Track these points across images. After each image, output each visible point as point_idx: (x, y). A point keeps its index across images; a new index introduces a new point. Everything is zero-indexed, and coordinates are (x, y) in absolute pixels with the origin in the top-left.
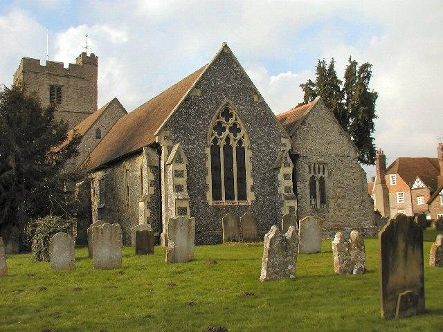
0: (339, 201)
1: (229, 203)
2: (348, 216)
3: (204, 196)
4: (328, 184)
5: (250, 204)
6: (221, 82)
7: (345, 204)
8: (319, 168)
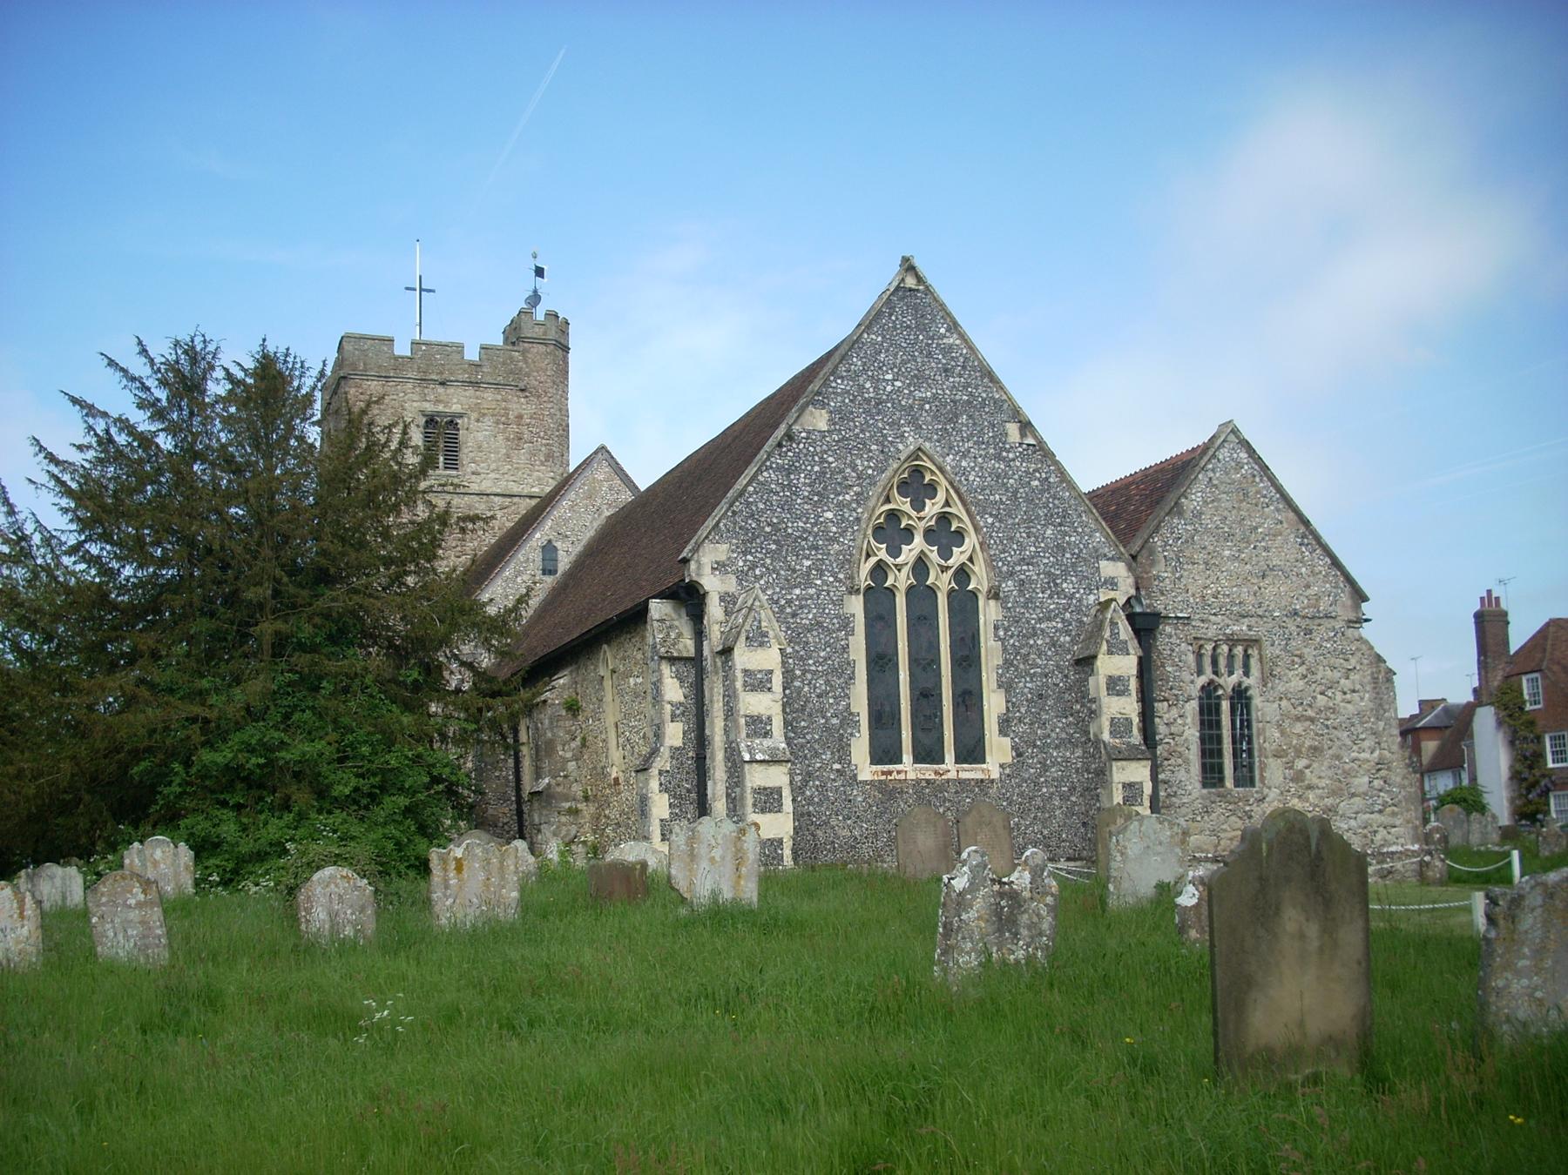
0: (1300, 764)
1: (927, 771)
5: (995, 775)
6: (898, 384)
8: (1231, 657)
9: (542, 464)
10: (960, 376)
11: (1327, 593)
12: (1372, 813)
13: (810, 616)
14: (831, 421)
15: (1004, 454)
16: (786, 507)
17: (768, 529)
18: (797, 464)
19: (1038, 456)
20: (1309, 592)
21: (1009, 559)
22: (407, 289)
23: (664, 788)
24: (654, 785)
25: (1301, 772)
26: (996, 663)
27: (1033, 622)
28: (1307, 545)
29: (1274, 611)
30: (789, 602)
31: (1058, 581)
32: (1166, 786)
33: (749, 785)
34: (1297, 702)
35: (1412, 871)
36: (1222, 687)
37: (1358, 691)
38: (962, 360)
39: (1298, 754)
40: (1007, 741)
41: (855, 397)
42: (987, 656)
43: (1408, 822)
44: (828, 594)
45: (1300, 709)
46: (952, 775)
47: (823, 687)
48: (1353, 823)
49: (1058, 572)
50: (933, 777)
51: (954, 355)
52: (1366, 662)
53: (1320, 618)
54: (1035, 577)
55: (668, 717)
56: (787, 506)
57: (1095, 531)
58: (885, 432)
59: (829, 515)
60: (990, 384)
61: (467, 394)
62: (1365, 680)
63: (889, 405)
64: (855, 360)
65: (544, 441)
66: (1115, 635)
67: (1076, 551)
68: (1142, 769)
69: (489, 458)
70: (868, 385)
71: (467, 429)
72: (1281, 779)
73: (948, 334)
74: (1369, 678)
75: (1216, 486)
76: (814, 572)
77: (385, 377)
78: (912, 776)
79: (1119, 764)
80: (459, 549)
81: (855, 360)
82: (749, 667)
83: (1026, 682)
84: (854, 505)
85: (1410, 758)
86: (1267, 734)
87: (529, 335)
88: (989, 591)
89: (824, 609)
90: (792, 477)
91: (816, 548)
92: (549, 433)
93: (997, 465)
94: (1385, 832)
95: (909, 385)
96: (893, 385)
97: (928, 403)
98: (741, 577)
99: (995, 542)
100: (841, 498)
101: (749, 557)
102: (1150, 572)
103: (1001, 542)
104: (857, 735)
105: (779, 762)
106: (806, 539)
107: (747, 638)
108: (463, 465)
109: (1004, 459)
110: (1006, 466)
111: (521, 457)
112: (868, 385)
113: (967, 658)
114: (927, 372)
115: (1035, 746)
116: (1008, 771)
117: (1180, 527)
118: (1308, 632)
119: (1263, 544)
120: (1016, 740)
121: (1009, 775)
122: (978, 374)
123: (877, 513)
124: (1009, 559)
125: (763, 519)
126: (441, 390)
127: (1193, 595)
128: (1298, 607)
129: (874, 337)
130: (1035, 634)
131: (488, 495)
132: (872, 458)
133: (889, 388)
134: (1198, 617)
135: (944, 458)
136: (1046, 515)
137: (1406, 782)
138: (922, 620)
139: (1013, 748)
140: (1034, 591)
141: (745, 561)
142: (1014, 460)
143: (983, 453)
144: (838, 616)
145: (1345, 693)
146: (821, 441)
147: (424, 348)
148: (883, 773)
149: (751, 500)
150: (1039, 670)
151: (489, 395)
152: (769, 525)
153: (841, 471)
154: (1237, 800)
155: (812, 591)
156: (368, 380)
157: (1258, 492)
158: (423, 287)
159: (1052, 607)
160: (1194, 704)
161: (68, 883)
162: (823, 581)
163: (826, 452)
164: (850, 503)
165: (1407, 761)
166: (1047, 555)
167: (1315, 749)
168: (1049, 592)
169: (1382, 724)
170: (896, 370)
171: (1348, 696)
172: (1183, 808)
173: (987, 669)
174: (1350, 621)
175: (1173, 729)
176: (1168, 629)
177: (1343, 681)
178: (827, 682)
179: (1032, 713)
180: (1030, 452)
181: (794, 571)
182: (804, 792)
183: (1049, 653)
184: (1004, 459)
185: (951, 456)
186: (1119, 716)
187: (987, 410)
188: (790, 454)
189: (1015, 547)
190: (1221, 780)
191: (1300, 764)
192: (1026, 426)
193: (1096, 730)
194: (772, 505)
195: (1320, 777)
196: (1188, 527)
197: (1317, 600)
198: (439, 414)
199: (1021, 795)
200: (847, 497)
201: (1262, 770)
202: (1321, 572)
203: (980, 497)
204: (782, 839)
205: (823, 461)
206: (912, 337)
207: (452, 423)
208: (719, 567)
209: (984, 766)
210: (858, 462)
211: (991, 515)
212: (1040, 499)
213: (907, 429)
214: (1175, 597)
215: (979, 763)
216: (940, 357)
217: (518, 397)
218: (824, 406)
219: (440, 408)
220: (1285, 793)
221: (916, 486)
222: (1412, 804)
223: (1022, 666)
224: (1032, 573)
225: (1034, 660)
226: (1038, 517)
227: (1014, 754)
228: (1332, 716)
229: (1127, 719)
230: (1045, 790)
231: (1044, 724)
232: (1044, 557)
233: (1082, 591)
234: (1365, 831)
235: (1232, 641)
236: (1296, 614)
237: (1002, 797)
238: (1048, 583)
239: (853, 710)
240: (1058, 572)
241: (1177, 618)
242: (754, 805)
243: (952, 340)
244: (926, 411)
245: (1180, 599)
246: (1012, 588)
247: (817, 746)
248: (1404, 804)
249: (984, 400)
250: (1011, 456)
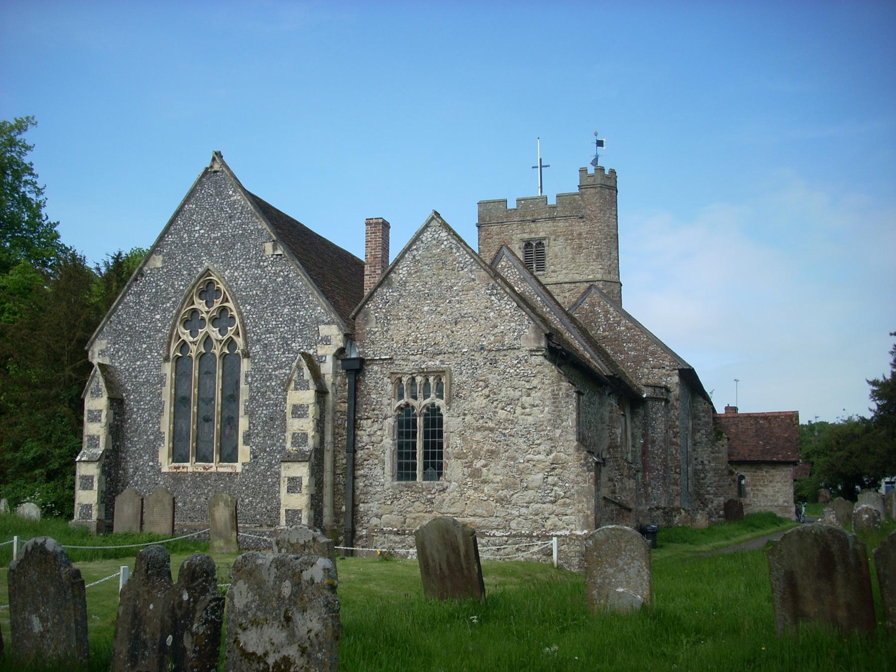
0: (478, 464)
1: (200, 467)
2: (501, 500)
3: (154, 455)
4: (450, 422)
5: (239, 470)
6: (202, 231)
7: (496, 472)
8: (427, 383)
9: (594, 260)
10: (239, 219)
11: (512, 330)
12: (544, 503)
13: (144, 377)
14: (164, 261)
15: (261, 263)
16: (137, 315)
17: (127, 329)
18: (144, 289)
20: (496, 330)
21: (258, 331)
22: (533, 167)
25: (479, 470)
26: (245, 398)
27: (270, 370)
28: (496, 294)
29: (463, 348)
30: (134, 369)
31: (289, 342)
32: (364, 479)
34: (479, 417)
35: (576, 552)
37: (537, 406)
38: (240, 208)
39: (477, 456)
40: (248, 448)
41: (177, 244)
43: (579, 512)
44: (154, 364)
45: (481, 421)
47: (147, 418)
48: (524, 510)
49: (290, 336)
50: (202, 470)
51: (236, 206)
52: (547, 382)
53: (505, 350)
54: (274, 341)
56: (137, 314)
58: (192, 262)
60: (257, 221)
61: (548, 225)
62: (546, 397)
63: (196, 245)
64: (179, 222)
65: (595, 247)
66: (301, 376)
67: (303, 321)
68: (302, 468)
69: (562, 261)
70: (185, 236)
71: (548, 246)
72: (461, 475)
73: (234, 194)
74: (550, 394)
76: (147, 351)
77: (501, 223)
78: (190, 470)
79: (286, 464)
81: (179, 222)
82: (92, 408)
83: (263, 410)
84: (171, 309)
85: (585, 459)
86: (451, 441)
87: (584, 184)
89: (151, 372)
90: (141, 297)
91: (149, 337)
92: (598, 241)
93: (256, 272)
94: (557, 518)
95: (208, 231)
96: (199, 233)
97: (218, 240)
98: (112, 356)
99: (250, 321)
100: (165, 306)
101: (117, 346)
102: (364, 329)
103: (254, 321)
104: (163, 445)
105: (92, 462)
106: (145, 332)
107: (91, 392)
109: (261, 267)
110: (261, 271)
111: (581, 259)
113: (231, 398)
114: (219, 221)
115: (265, 451)
116: (247, 468)
117: (388, 294)
118: (494, 362)
119: (457, 298)
120: (254, 447)
121: (247, 470)
122: (250, 215)
123: (183, 312)
124: (258, 331)
125: (124, 324)
126: (533, 225)
127: (397, 342)
128: (485, 343)
129: (191, 206)
130: (271, 379)
131: (561, 283)
132: (183, 279)
133: (197, 235)
134: (399, 357)
135: (224, 272)
136: (285, 300)
137: (580, 479)
138: (207, 373)
139: (251, 453)
140: (273, 350)
142: (267, 266)
143: (248, 265)
144: (157, 376)
145: (524, 408)
146: (157, 274)
147: (523, 202)
148: (175, 468)
149: (120, 313)
150: (272, 402)
152: (127, 326)
153: (166, 289)
154: (421, 491)
155: (146, 362)
157: (454, 260)
158: (543, 165)
159: (284, 360)
160: (390, 421)
162: (152, 356)
163: (159, 280)
164: (169, 308)
165: (582, 461)
166: (283, 325)
167: (492, 452)
168: (282, 350)
169: (558, 432)
170: (201, 223)
171: (527, 410)
172: (377, 495)
174: (531, 351)
175: (373, 439)
176: (376, 368)
177: (524, 398)
178: (150, 415)
179: (265, 430)
180: (278, 260)
181: (138, 351)
182: (133, 478)
183: (279, 390)
184: (261, 267)
185: (228, 271)
186: (299, 432)
187: (253, 237)
188: (141, 284)
189: (263, 323)
190: (414, 477)
191: (478, 464)
194: (130, 315)
195: (495, 474)
196: (395, 294)
197: (502, 336)
198: (532, 239)
199: (254, 483)
200: (168, 305)
202: (507, 315)
203: (244, 294)
204: (92, 504)
205: (157, 285)
206: (212, 201)
207: (540, 244)
211: (249, 304)
212: (282, 289)
213: (205, 258)
214: (382, 344)
215: (186, 462)
216: (228, 210)
217: (579, 222)
218: (160, 252)
219: (533, 236)
220: (463, 486)
221: (208, 290)
222: (585, 496)
223: (261, 400)
224: (272, 338)
225: (269, 395)
226: (279, 302)
227: (252, 456)
228: (510, 427)
229: (304, 434)
230: (270, 480)
231: (272, 437)
232: (281, 327)
233: (305, 347)
234: (536, 517)
235: (426, 374)
236: (482, 348)
237: (242, 484)
238: (283, 344)
239: (162, 430)
240: (290, 336)
241: (381, 359)
243: (235, 197)
244: (217, 245)
245: (385, 346)
246: (259, 350)
247: (141, 452)
248: (576, 496)
249: (252, 231)
250: (265, 264)
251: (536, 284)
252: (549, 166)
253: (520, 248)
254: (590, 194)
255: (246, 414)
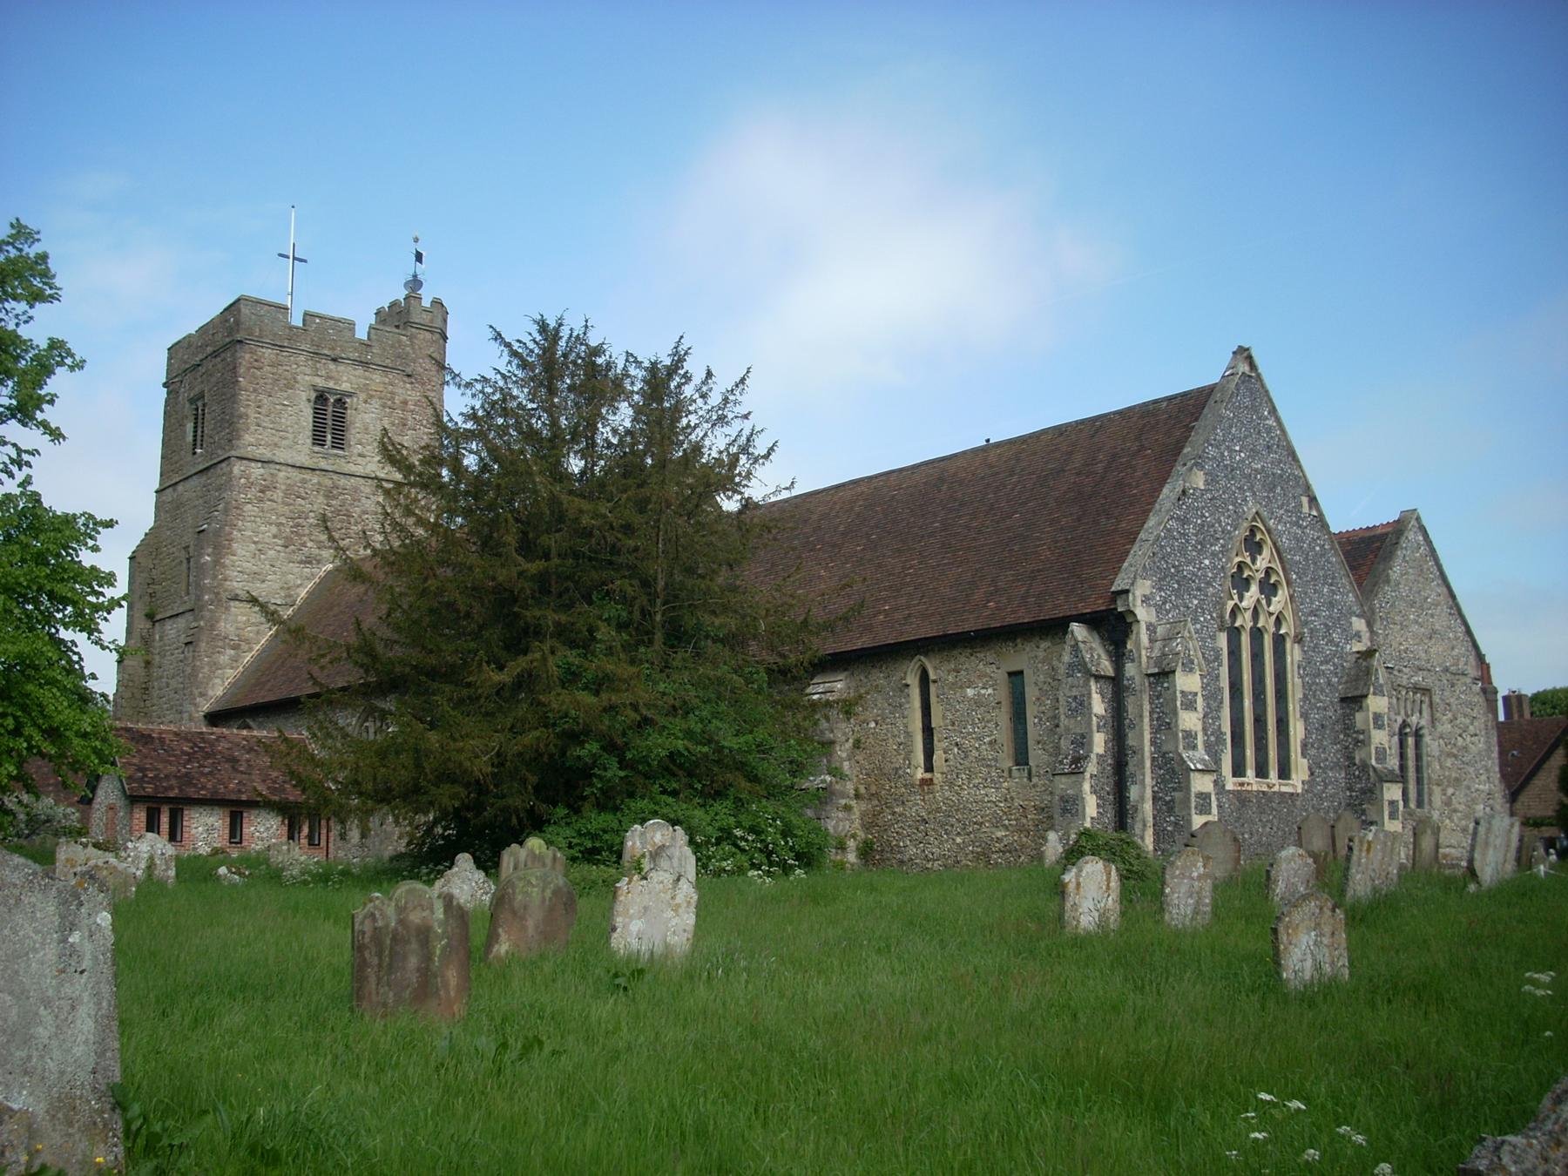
10: (1276, 453)
14: (1207, 483)
17: (1173, 570)
19: (1318, 526)
22: (281, 255)
23: (1094, 792)
24: (1087, 787)
33: (1193, 790)
36: (1409, 725)
40: (1306, 761)
42: (1293, 691)
46: (1276, 789)
55: (1095, 728)
57: (1349, 592)
59: (1207, 562)
61: (357, 373)
71: (356, 409)
75: (1407, 562)
77: (280, 346)
80: (343, 531)
82: (1186, 689)
87: (417, 321)
88: (1296, 636)
91: (1199, 589)
106: (1194, 582)
107: (1183, 664)
108: (350, 446)
112: (1226, 454)
126: (332, 366)
141: (1161, 596)
147: (318, 321)
151: (377, 377)
156: (262, 347)
161: (683, 863)
173: (1294, 700)
181: (1188, 608)
192: (1313, 500)
193: (1363, 756)
201: (1430, 795)
207: (340, 402)
208: (1146, 600)
209: (1290, 782)
210: (1222, 518)
217: (404, 382)
218: (1202, 468)
219: (331, 384)
242: (1196, 808)
251: (309, 471)
252: (305, 261)
253: (309, 400)
254: (424, 339)
255: (1301, 716)
